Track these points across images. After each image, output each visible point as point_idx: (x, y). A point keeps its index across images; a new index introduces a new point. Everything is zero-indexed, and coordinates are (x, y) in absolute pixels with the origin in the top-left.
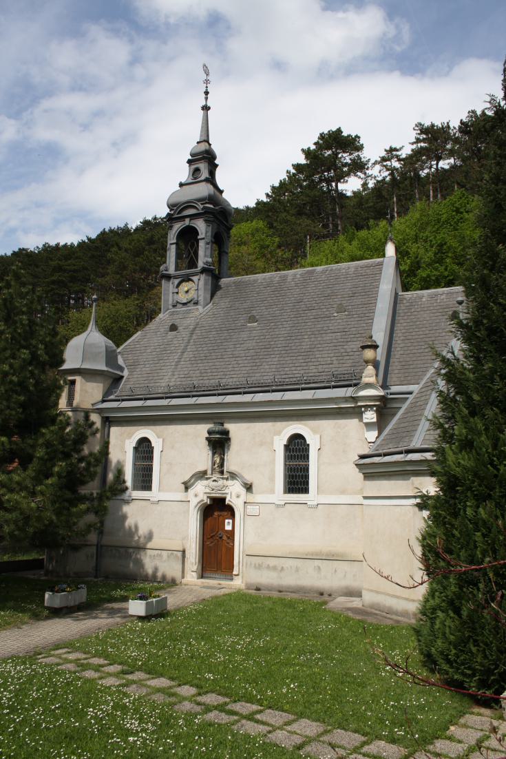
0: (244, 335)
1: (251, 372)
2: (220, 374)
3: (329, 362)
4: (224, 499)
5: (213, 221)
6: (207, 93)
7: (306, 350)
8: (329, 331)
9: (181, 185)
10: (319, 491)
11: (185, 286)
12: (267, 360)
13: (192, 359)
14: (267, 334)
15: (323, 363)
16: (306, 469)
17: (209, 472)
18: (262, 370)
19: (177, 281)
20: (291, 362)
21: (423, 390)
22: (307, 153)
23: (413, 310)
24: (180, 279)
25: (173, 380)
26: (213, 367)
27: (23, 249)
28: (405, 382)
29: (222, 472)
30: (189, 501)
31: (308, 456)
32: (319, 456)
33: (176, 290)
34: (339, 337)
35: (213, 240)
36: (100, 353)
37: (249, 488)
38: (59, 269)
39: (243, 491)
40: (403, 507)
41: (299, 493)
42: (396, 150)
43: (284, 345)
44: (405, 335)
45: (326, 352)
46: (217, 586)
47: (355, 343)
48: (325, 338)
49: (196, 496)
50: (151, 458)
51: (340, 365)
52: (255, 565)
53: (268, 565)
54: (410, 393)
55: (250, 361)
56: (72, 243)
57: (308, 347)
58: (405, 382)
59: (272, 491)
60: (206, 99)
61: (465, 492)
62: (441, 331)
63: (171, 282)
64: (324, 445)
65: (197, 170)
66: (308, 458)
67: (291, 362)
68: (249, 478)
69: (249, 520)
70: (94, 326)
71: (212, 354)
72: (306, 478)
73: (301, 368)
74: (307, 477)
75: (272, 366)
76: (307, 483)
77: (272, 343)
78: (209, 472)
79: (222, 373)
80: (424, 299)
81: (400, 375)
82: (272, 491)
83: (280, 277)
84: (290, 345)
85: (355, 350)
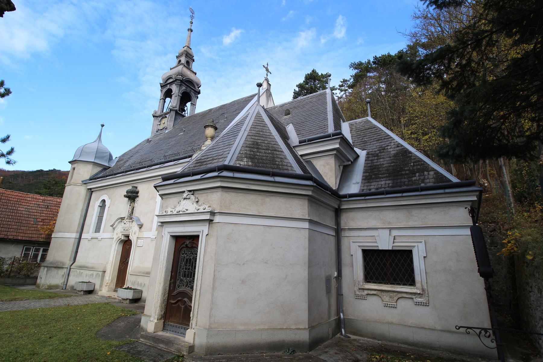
9: (171, 69)
17: (126, 218)
19: (160, 118)
24: (160, 118)
27: (384, 55)
30: (113, 238)
33: (159, 123)
36: (105, 156)
37: (141, 226)
38: (311, 102)
56: (408, 46)
68: (142, 221)
69: (138, 249)
78: (126, 218)
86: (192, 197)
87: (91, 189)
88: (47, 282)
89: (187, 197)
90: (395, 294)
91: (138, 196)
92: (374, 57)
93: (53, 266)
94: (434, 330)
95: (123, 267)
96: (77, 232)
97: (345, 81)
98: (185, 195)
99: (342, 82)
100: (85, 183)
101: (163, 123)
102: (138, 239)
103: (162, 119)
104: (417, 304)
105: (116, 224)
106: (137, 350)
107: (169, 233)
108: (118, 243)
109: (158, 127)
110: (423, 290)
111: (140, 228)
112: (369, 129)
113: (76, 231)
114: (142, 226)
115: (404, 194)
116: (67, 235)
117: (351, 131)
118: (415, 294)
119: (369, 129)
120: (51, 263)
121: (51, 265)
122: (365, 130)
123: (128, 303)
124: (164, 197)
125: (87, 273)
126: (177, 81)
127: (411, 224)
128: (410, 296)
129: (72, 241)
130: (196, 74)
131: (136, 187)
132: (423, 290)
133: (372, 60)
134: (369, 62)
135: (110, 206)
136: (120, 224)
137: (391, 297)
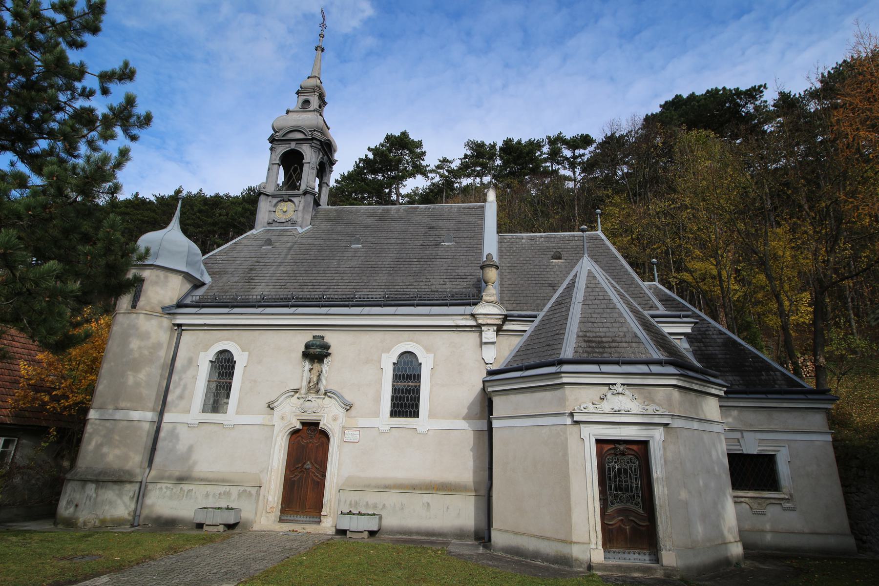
0: (348, 254)
2: (322, 287)
3: (442, 283)
4: (318, 424)
5: (320, 149)
8: (438, 257)
9: (288, 112)
10: (432, 415)
11: (285, 206)
12: (375, 278)
13: (290, 272)
16: (417, 391)
17: (303, 391)
18: (370, 287)
19: (275, 201)
21: (554, 308)
22: (375, 151)
24: (279, 199)
29: (317, 391)
32: (432, 375)
34: (450, 262)
35: (318, 167)
39: (340, 412)
40: (553, 428)
41: (406, 417)
42: (448, 161)
44: (510, 268)
46: (304, 528)
48: (434, 263)
50: (231, 375)
51: (454, 286)
52: (351, 502)
53: (367, 503)
57: (418, 269)
59: (376, 414)
62: (545, 267)
63: (269, 200)
64: (437, 365)
65: (307, 102)
68: (349, 398)
70: (177, 222)
73: (413, 287)
75: (380, 284)
76: (417, 406)
80: (523, 241)
81: (511, 302)
82: (376, 414)
83: (383, 210)
86: (627, 392)
87: (179, 325)
88: (98, 513)
89: (623, 393)
90: (763, 500)
91: (329, 354)
93: (111, 478)
94: (803, 533)
95: (298, 477)
96: (154, 410)
97: (445, 161)
99: (440, 161)
100: (169, 311)
101: (285, 210)
102: (345, 429)
104: (785, 509)
105: (281, 399)
107: (593, 435)
108: (288, 433)
110: (791, 495)
111: (347, 410)
114: (351, 407)
115: (770, 396)
116: (135, 415)
118: (782, 499)
120: (100, 474)
121: (106, 478)
123: (366, 537)
124: (723, 409)
125: (207, 492)
126: (315, 141)
127: (773, 427)
128: (779, 502)
129: (146, 426)
130: (329, 129)
131: (323, 338)
132: (791, 495)
133: (500, 144)
134: (493, 146)
135: (248, 362)
136: (288, 400)
137: (759, 504)
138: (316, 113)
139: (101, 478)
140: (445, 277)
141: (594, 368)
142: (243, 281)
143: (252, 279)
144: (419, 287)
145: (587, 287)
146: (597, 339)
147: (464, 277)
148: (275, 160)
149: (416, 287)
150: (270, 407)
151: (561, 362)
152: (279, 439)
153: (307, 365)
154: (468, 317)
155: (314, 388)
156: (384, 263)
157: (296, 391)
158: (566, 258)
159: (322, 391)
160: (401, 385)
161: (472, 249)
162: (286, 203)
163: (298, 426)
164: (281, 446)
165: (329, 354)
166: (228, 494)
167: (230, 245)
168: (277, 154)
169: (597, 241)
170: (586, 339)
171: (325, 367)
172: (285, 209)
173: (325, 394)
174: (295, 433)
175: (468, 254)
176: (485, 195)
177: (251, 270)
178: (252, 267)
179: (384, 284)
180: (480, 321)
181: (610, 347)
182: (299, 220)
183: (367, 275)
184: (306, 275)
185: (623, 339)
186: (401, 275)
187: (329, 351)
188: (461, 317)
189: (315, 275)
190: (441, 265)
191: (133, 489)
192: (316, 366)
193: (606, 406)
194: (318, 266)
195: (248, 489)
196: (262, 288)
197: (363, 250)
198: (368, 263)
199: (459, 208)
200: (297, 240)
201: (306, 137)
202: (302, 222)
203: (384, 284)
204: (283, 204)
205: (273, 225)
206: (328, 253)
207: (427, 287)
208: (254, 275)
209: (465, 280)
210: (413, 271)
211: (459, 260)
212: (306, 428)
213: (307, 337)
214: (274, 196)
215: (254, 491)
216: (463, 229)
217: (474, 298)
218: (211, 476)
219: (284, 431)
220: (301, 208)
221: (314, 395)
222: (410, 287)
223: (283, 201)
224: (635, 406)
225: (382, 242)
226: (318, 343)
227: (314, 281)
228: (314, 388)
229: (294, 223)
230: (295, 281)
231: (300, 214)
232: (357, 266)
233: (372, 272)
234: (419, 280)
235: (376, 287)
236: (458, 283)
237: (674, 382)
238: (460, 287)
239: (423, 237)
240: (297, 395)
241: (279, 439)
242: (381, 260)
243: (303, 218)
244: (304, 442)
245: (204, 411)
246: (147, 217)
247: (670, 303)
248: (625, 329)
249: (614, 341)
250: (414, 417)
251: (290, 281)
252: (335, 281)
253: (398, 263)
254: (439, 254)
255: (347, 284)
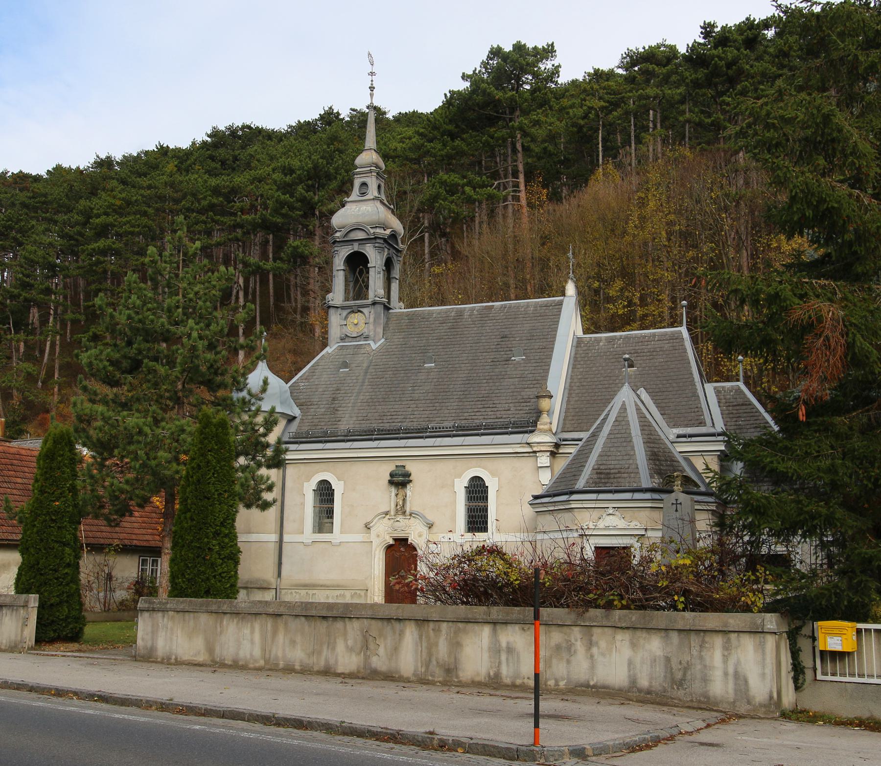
1: (431, 416)
2: (399, 417)
3: (507, 408)
4: (407, 540)
6: (372, 88)
7: (485, 395)
11: (356, 318)
12: (447, 404)
14: (445, 376)
15: (501, 409)
16: (486, 509)
17: (392, 513)
18: (442, 415)
19: (345, 313)
20: (470, 407)
21: (590, 439)
23: (590, 355)
24: (349, 310)
25: (352, 422)
26: (392, 410)
28: (578, 429)
29: (404, 513)
31: (487, 497)
32: (497, 497)
39: (425, 530)
43: (463, 389)
45: (504, 398)
47: (532, 390)
49: (378, 536)
50: (332, 501)
51: (517, 412)
54: (580, 440)
55: (429, 405)
57: (486, 392)
58: (578, 429)
60: (372, 95)
61: (44, 328)
62: (615, 378)
63: (338, 313)
66: (487, 499)
67: (470, 407)
68: (431, 518)
71: (390, 396)
72: (485, 493)
73: (480, 413)
74: (486, 517)
75: (452, 411)
77: (452, 386)
79: (403, 417)
80: (601, 344)
81: (573, 422)
84: (469, 389)
85: (531, 397)
86: (617, 513)
91: (411, 481)
92: (688, 45)
98: (611, 511)
101: (356, 322)
103: (350, 313)
105: (375, 521)
106: (710, 596)
109: (344, 331)
111: (430, 528)
112: (743, 405)
113: (273, 530)
117: (719, 402)
119: (743, 405)
120: (247, 582)
121: (252, 586)
122: (738, 405)
126: (378, 241)
131: (404, 467)
138: (375, 201)
139: (249, 586)
140: (510, 401)
141: (593, 496)
142: (329, 413)
143: (337, 410)
144: (486, 413)
145: (616, 421)
146: (607, 471)
147: (528, 400)
148: (339, 265)
149: (483, 413)
150: (367, 527)
151: (572, 493)
152: (377, 552)
153: (393, 490)
154: (524, 445)
155: (401, 510)
156: (455, 386)
157: (387, 513)
158: (638, 365)
159: (408, 513)
160: (474, 504)
161: (541, 364)
162: (356, 314)
163: (392, 542)
164: (379, 558)
165: (411, 481)
166: (343, 596)
167: (309, 369)
168: (341, 257)
169: (678, 340)
170: (599, 471)
171: (409, 490)
172: (356, 321)
173: (410, 515)
174: (389, 548)
175: (536, 372)
176: (564, 287)
177: (334, 399)
178: (334, 396)
179: (454, 411)
180: (535, 449)
181: (614, 478)
182: (372, 334)
183: (440, 401)
184: (385, 403)
185: (627, 471)
186: (470, 400)
187: (411, 478)
188: (519, 446)
189: (391, 403)
190: (507, 387)
191: (271, 594)
192: (401, 492)
193: (601, 524)
194: (394, 393)
195: (358, 592)
196: (346, 424)
197: (436, 370)
198: (440, 387)
199: (536, 305)
200: (372, 360)
201: (368, 237)
202: (375, 336)
203: (454, 411)
204: (353, 315)
205: (346, 340)
206: (402, 375)
207: (492, 413)
208: (337, 405)
209: (528, 404)
210: (482, 395)
211: (526, 379)
212: (398, 543)
213: (390, 467)
214: (343, 308)
215: (362, 593)
216: (535, 337)
217: (528, 426)
218: (328, 583)
219: (380, 547)
220: (372, 320)
221: (401, 517)
222: (477, 414)
223: (353, 312)
224: (622, 524)
225: (454, 359)
226: (400, 473)
227: (392, 410)
228: (401, 510)
229: (367, 338)
230: (374, 411)
231: (371, 327)
232: (430, 391)
233: (444, 397)
234: (486, 406)
235: (447, 415)
236: (521, 408)
237: (650, 505)
238: (517, 414)
239: (494, 350)
240: (388, 517)
241: (377, 552)
242: (453, 383)
243: (375, 331)
244: (397, 555)
245: (314, 532)
246: (139, 226)
247: (744, 407)
248: (631, 461)
249: (619, 472)
250: (485, 532)
251: (371, 411)
252: (410, 409)
253: (469, 385)
254: (508, 373)
255: (421, 412)
